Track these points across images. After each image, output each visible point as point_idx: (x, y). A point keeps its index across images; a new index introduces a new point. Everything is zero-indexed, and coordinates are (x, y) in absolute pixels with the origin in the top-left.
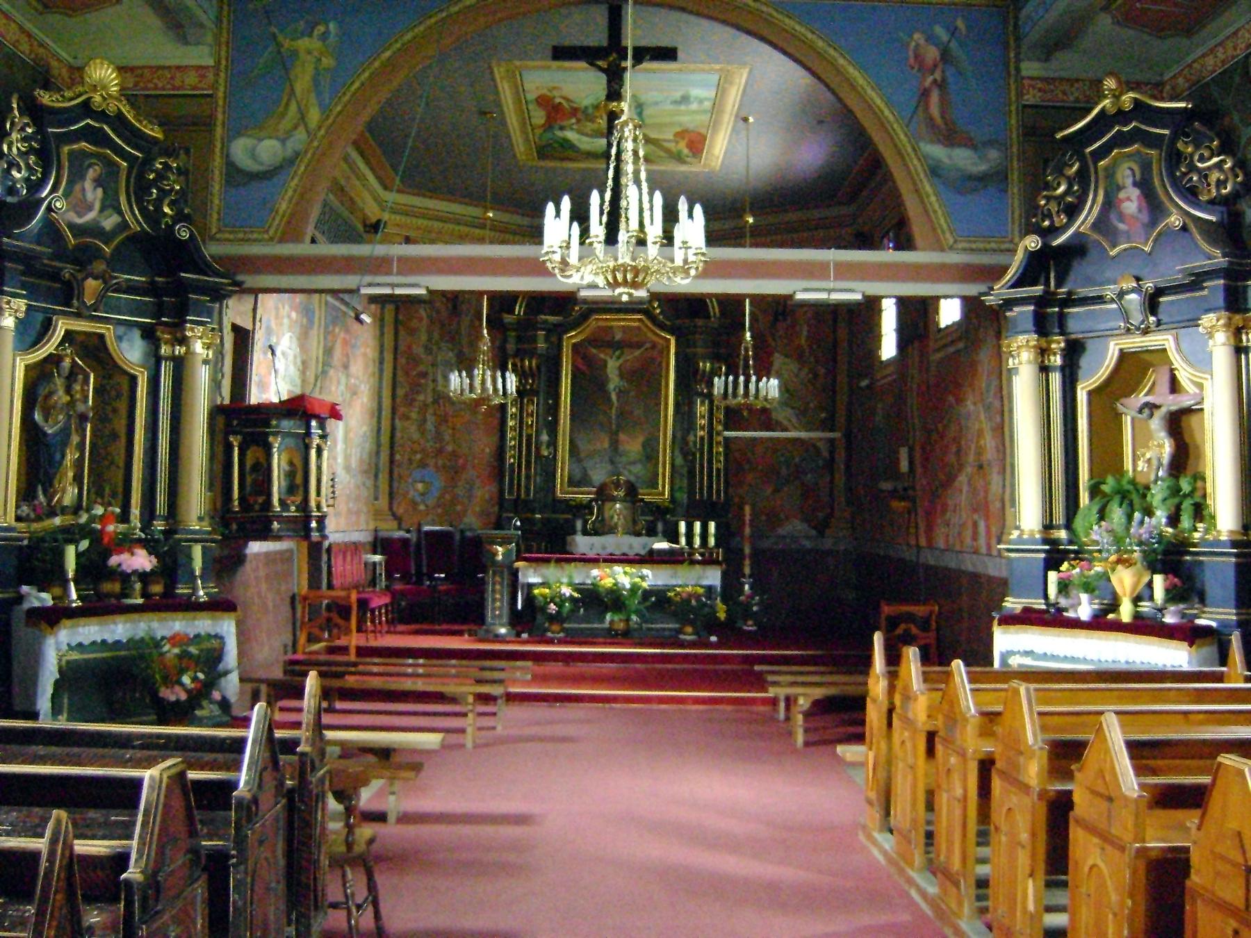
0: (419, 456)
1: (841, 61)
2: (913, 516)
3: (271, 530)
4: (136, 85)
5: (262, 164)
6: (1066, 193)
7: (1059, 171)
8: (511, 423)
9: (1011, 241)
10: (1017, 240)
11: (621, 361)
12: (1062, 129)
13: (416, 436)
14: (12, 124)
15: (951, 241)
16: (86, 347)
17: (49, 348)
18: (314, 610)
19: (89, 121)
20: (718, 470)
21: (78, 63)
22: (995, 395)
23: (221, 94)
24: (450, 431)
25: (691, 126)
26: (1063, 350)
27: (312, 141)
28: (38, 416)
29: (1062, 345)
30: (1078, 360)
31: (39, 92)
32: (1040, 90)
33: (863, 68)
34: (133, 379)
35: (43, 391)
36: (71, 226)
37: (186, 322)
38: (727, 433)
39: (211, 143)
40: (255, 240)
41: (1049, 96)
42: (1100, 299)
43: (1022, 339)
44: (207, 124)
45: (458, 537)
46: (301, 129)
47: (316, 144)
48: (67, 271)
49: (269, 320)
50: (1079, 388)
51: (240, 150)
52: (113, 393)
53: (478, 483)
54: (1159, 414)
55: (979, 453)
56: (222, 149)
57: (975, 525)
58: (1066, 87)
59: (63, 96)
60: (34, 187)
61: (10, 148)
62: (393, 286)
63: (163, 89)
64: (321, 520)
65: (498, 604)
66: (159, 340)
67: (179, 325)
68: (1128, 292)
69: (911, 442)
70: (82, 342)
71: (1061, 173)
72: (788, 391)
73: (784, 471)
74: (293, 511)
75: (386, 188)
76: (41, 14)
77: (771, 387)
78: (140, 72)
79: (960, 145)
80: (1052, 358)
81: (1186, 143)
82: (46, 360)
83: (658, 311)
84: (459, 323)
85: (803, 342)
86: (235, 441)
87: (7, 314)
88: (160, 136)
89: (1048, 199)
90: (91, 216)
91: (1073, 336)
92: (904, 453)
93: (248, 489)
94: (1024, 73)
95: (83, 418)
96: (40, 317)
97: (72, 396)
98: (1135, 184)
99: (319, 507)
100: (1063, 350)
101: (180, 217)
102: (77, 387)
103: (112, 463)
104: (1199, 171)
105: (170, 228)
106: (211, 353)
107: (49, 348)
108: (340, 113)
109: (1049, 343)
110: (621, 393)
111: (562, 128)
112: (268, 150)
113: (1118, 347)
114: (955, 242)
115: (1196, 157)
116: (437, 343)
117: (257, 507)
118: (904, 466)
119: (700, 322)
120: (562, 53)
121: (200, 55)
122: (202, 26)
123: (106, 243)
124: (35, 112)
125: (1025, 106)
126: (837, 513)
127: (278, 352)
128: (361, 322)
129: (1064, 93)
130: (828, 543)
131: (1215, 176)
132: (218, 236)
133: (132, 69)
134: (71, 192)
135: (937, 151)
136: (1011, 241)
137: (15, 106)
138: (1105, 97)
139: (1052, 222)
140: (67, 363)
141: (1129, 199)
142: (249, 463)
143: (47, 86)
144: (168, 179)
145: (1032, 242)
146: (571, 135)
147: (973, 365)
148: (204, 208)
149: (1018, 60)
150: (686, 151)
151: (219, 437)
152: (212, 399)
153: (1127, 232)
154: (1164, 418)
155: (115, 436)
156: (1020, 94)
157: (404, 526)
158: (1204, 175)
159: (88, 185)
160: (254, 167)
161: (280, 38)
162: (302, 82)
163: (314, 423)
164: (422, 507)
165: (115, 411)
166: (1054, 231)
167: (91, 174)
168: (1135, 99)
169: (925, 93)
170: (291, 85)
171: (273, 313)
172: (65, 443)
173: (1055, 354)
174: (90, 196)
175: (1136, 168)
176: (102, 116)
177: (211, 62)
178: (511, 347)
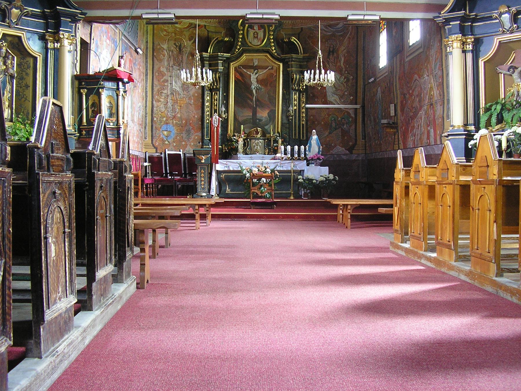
0: (164, 119)
2: (397, 136)
8: (207, 104)
13: (163, 110)
22: (439, 69)
24: (179, 107)
26: (472, 42)
29: (473, 40)
34: (35, 59)
37: (60, 30)
42: (490, 18)
43: (454, 37)
50: (480, 60)
52: (26, 66)
53: (193, 131)
55: (430, 99)
57: (429, 132)
65: (203, 183)
66: (47, 40)
67: (56, 32)
69: (396, 102)
70: (10, 41)
73: (334, 125)
74: (111, 125)
80: (468, 46)
84: (182, 58)
86: (84, 92)
91: (477, 36)
92: (392, 107)
93: (90, 114)
95: (12, 77)
97: (6, 66)
100: (472, 42)
102: (9, 62)
103: (26, 99)
109: (466, 39)
110: (257, 90)
116: (172, 67)
118: (392, 113)
119: (294, 56)
127: (101, 58)
128: (137, 53)
130: (354, 157)
147: (427, 58)
151: (76, 90)
155: (27, 86)
163: (120, 83)
164: (167, 142)
171: (99, 37)
173: (469, 44)
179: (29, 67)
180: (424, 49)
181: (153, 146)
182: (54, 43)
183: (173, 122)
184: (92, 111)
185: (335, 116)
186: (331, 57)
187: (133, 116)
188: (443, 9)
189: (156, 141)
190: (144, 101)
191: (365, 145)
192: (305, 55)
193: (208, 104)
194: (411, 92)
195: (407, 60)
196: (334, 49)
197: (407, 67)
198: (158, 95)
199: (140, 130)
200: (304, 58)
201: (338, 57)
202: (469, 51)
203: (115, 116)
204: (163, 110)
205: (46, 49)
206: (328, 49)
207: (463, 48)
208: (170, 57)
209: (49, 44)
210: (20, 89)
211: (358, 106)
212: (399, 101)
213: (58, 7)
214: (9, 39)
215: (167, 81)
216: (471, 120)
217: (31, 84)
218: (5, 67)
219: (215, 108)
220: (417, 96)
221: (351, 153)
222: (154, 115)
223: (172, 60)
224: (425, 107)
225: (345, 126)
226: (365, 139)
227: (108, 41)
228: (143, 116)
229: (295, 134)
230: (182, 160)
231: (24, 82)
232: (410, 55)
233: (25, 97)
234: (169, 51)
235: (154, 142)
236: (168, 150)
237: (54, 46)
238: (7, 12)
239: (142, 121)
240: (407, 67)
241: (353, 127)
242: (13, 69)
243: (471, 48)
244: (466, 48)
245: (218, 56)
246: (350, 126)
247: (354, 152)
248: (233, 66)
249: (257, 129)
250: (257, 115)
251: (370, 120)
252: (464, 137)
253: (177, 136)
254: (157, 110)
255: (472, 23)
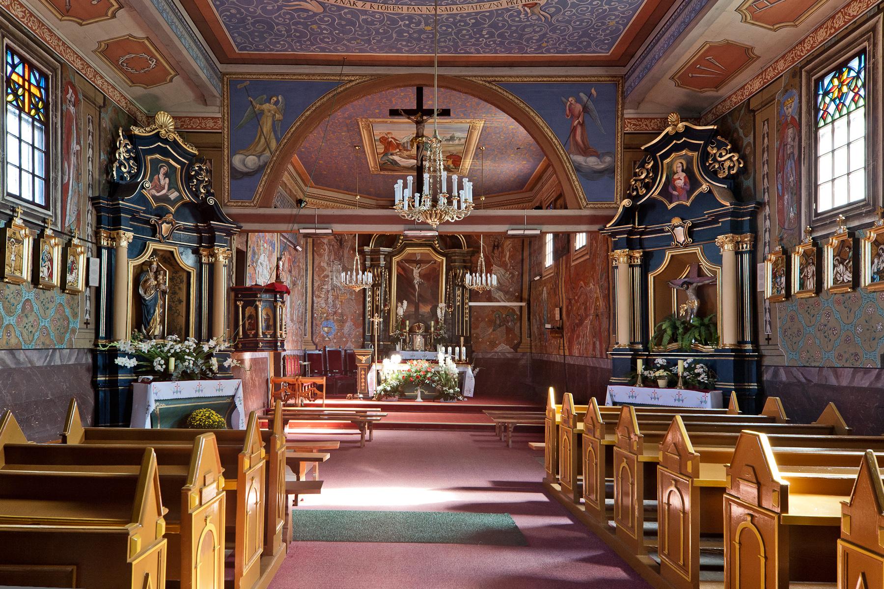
0: (325, 315)
1: (532, 114)
3: (258, 347)
4: (182, 126)
5: (249, 168)
6: (646, 177)
7: (642, 166)
8: (368, 299)
9: (616, 203)
10: (618, 203)
11: (420, 270)
12: (644, 145)
13: (324, 306)
14: (120, 143)
15: (585, 204)
16: (164, 258)
17: (145, 258)
18: (277, 386)
19: (159, 143)
20: (466, 321)
21: (152, 114)
22: (605, 280)
23: (226, 132)
25: (455, 153)
27: (273, 157)
28: (141, 292)
30: (649, 262)
31: (132, 127)
32: (634, 125)
33: (542, 116)
34: (189, 274)
35: (143, 279)
36: (154, 197)
37: (214, 246)
38: (471, 304)
39: (222, 155)
40: (247, 206)
41: (638, 128)
44: (219, 147)
45: (343, 353)
46: (268, 150)
47: (275, 158)
48: (153, 219)
49: (254, 247)
51: (237, 160)
52: (179, 280)
54: (691, 287)
56: (228, 160)
57: (594, 344)
58: (648, 122)
59: (145, 130)
60: (134, 177)
61: (120, 156)
62: (316, 229)
63: (195, 129)
64: (282, 342)
66: (201, 254)
67: (211, 245)
68: (677, 226)
70: (162, 256)
71: (644, 167)
72: (499, 282)
73: (498, 322)
74: (269, 338)
75: (306, 186)
76: (130, 86)
77: (494, 280)
78: (183, 119)
79: (591, 156)
80: (636, 260)
81: (712, 148)
82: (143, 263)
83: (438, 245)
84: (343, 252)
85: (507, 259)
86: (240, 304)
87: (123, 239)
88: (196, 153)
89: (636, 181)
90: (164, 192)
92: (557, 311)
94: (626, 116)
95: (164, 293)
96: (140, 242)
98: (683, 171)
99: (281, 335)
101: (209, 193)
102: (161, 277)
103: (179, 314)
104: (719, 162)
105: (204, 200)
106: (227, 261)
107: (145, 258)
108: (286, 143)
110: (420, 285)
111: (392, 154)
112: (252, 161)
113: (670, 255)
114: (587, 204)
115: (718, 155)
116: (333, 262)
117: (251, 336)
118: (557, 317)
119: (457, 250)
120: (394, 113)
121: (213, 111)
122: (214, 96)
123: (172, 207)
124: (131, 138)
125: (625, 133)
126: (523, 341)
128: (297, 250)
129: (646, 125)
131: (727, 164)
132: (228, 204)
133: (180, 118)
134: (153, 179)
135: (579, 159)
136: (616, 203)
137: (121, 134)
138: (670, 125)
139: (638, 192)
140: (155, 265)
141: (679, 179)
142: (247, 315)
143: (136, 125)
144: (201, 175)
145: (626, 202)
146: (396, 158)
148: (221, 189)
149: (623, 109)
150: (452, 166)
151: (232, 302)
152: (228, 284)
153: (678, 196)
154: (695, 289)
155: (180, 301)
156: (623, 127)
157: (318, 348)
158: (722, 164)
159: (161, 176)
160: (245, 170)
161: (254, 103)
162: (267, 127)
164: (327, 339)
165: (180, 289)
166: (639, 197)
167: (162, 171)
168: (686, 126)
169: (574, 129)
170: (261, 127)
172: (155, 305)
174: (162, 182)
175: (684, 163)
176: (165, 141)
177: (219, 115)
178: (368, 263)
179: (182, 282)
180: (590, 256)
181: (313, 342)
182: (208, 258)
183: (333, 319)
184: (249, 323)
185: (499, 313)
186: (496, 251)
187: (292, 315)
188: (609, 222)
189: (316, 337)
190: (304, 297)
191: (531, 344)
192: (468, 250)
193: (370, 299)
194: (576, 298)
195: (573, 264)
196: (498, 243)
197: (572, 271)
198: (318, 291)
199: (300, 328)
200: (468, 252)
201: (503, 252)
202: (637, 266)
203: (272, 328)
204: (324, 306)
205: (201, 264)
206: (493, 243)
207: (631, 262)
208: (330, 251)
209: (203, 259)
210: (172, 304)
211: (523, 304)
212: (564, 305)
213: (211, 222)
214: (161, 253)
215: (328, 276)
216: (638, 339)
217: (184, 299)
218: (156, 282)
219: (377, 304)
220: (583, 303)
221: (516, 352)
222: (314, 311)
223: (333, 255)
224: (591, 317)
225: (510, 324)
226: (530, 337)
227: (265, 245)
228: (302, 313)
229: (458, 331)
230: (342, 359)
231: (177, 297)
232: (577, 259)
233: (178, 312)
234: (330, 245)
235: (314, 338)
236: (329, 347)
237: (209, 260)
238: (157, 227)
239: (302, 318)
240: (572, 271)
241: (518, 324)
242: (165, 284)
243: (639, 263)
244: (634, 262)
245: (379, 251)
246: (515, 324)
247: (519, 350)
248: (395, 260)
249: (419, 325)
250: (420, 310)
251: (536, 320)
252: (630, 357)
253: (338, 333)
254: (317, 306)
255: (641, 235)
